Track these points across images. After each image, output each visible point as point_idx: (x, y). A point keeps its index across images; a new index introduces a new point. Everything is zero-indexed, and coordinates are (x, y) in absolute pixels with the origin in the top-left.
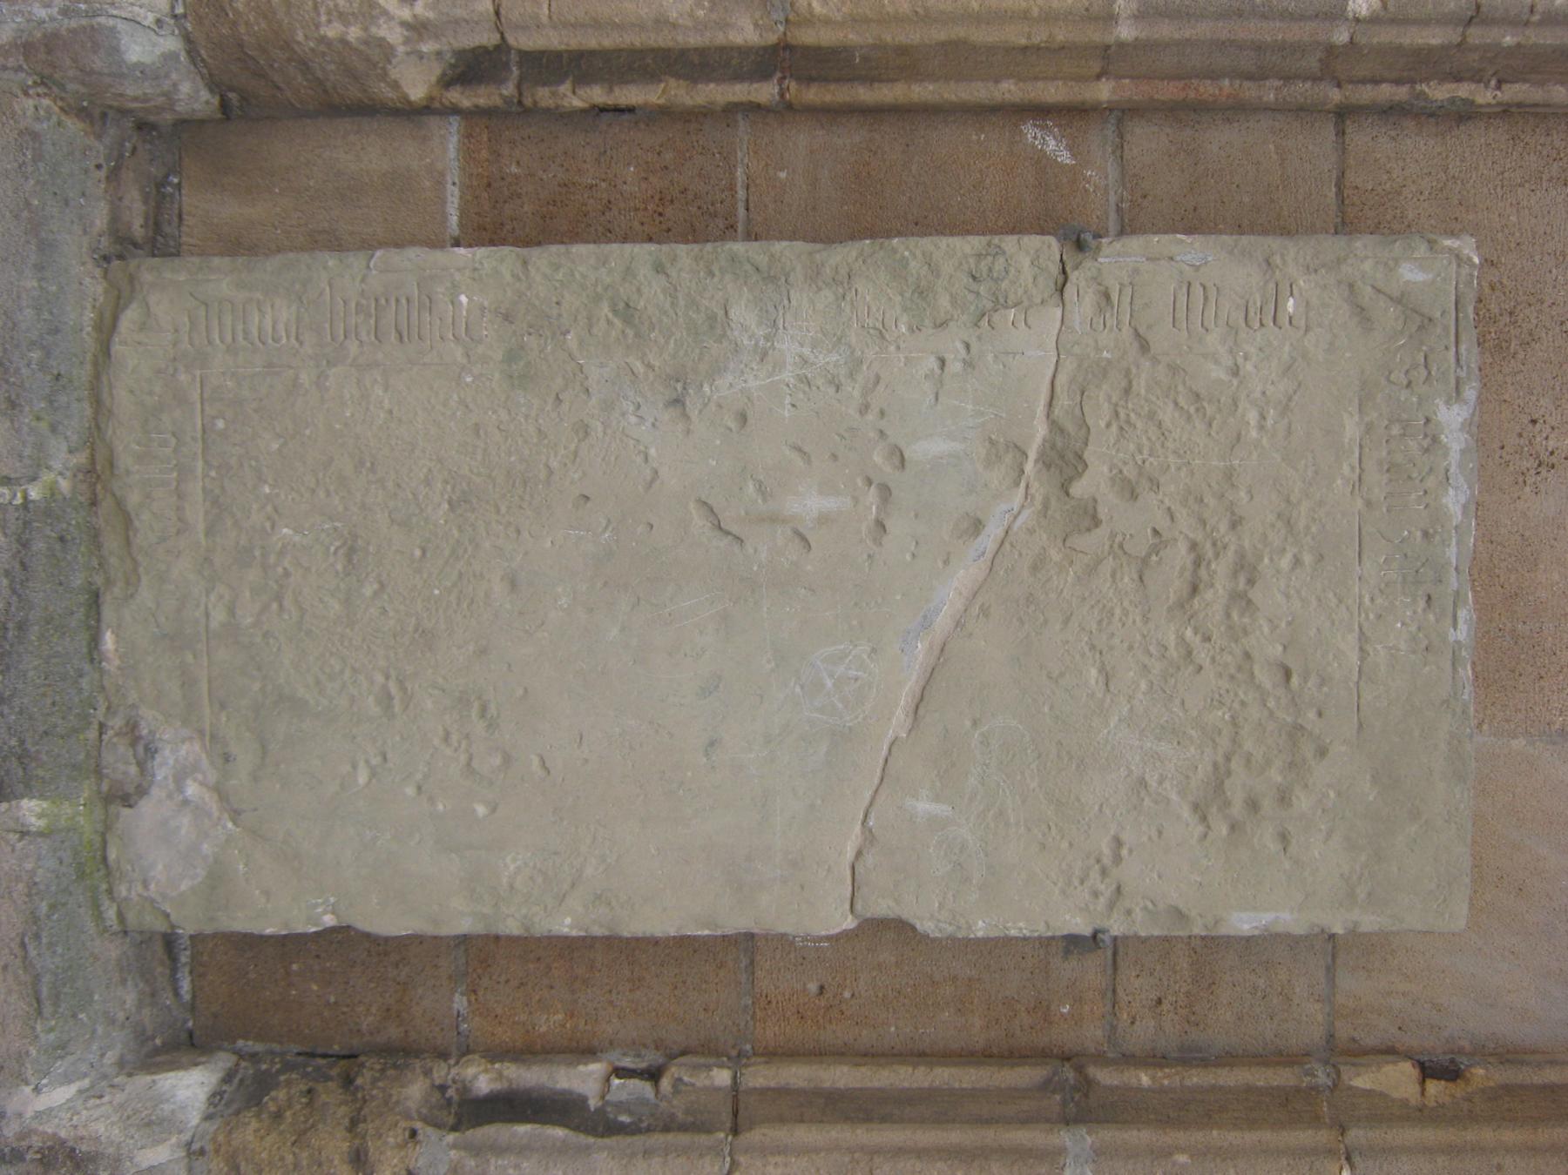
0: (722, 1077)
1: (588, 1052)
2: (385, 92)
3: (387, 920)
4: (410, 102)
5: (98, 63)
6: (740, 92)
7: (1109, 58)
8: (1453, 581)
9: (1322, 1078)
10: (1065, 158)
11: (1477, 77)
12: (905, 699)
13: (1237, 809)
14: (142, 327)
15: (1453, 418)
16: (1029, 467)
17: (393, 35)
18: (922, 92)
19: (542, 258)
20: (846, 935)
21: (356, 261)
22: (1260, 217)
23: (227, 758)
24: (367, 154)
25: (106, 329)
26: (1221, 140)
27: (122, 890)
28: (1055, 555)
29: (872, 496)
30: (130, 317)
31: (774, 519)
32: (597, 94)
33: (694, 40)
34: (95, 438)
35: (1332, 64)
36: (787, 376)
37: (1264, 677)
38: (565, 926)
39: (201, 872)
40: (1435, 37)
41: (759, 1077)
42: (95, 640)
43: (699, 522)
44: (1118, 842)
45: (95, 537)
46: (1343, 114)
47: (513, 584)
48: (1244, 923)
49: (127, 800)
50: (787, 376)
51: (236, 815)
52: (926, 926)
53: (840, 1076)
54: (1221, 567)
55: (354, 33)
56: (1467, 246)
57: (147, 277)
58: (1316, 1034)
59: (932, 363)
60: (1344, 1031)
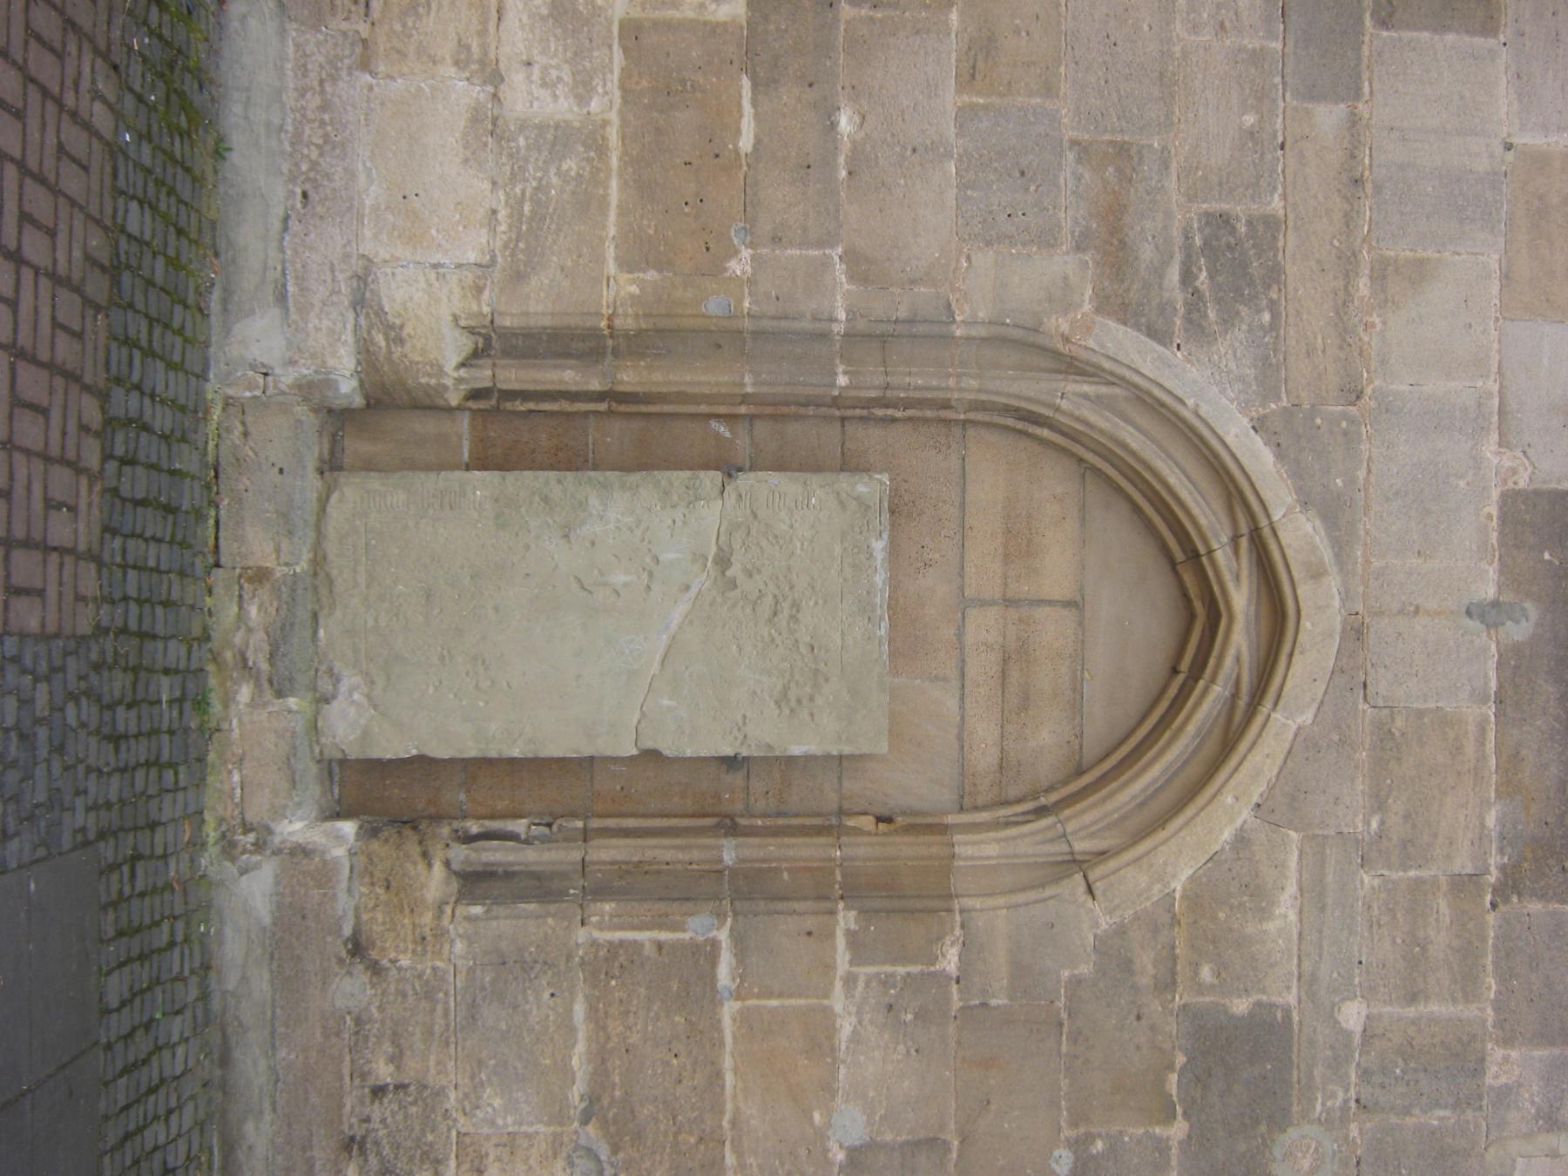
0: (580, 824)
1: (517, 816)
2: (441, 402)
3: (440, 751)
4: (1232, 1017)
5: (330, 394)
6: (591, 407)
7: (745, 399)
8: (879, 612)
9: (834, 821)
10: (728, 435)
11: (895, 407)
12: (658, 657)
13: (793, 703)
14: (341, 501)
15: (879, 546)
16: (709, 564)
17: (449, 382)
18: (667, 408)
19: (511, 476)
20: (632, 758)
21: (433, 475)
22: (810, 465)
23: (373, 683)
24: (427, 426)
25: (323, 502)
26: (792, 428)
27: (323, 740)
28: (719, 600)
29: (645, 576)
30: (335, 497)
31: (605, 584)
32: (531, 406)
33: (574, 388)
34: (318, 546)
35: (835, 402)
36: (611, 526)
37: (803, 650)
38: (516, 753)
39: (359, 732)
40: (873, 394)
41: (595, 823)
42: (315, 633)
43: (575, 586)
44: (745, 717)
45: (316, 588)
46: (843, 419)
47: (497, 609)
48: (796, 750)
49: (327, 701)
50: (611, 526)
51: (375, 707)
52: (667, 752)
53: (630, 823)
54: (786, 605)
55: (433, 381)
56: (885, 478)
57: (342, 480)
58: (835, 807)
59: (670, 522)
60: (846, 806)
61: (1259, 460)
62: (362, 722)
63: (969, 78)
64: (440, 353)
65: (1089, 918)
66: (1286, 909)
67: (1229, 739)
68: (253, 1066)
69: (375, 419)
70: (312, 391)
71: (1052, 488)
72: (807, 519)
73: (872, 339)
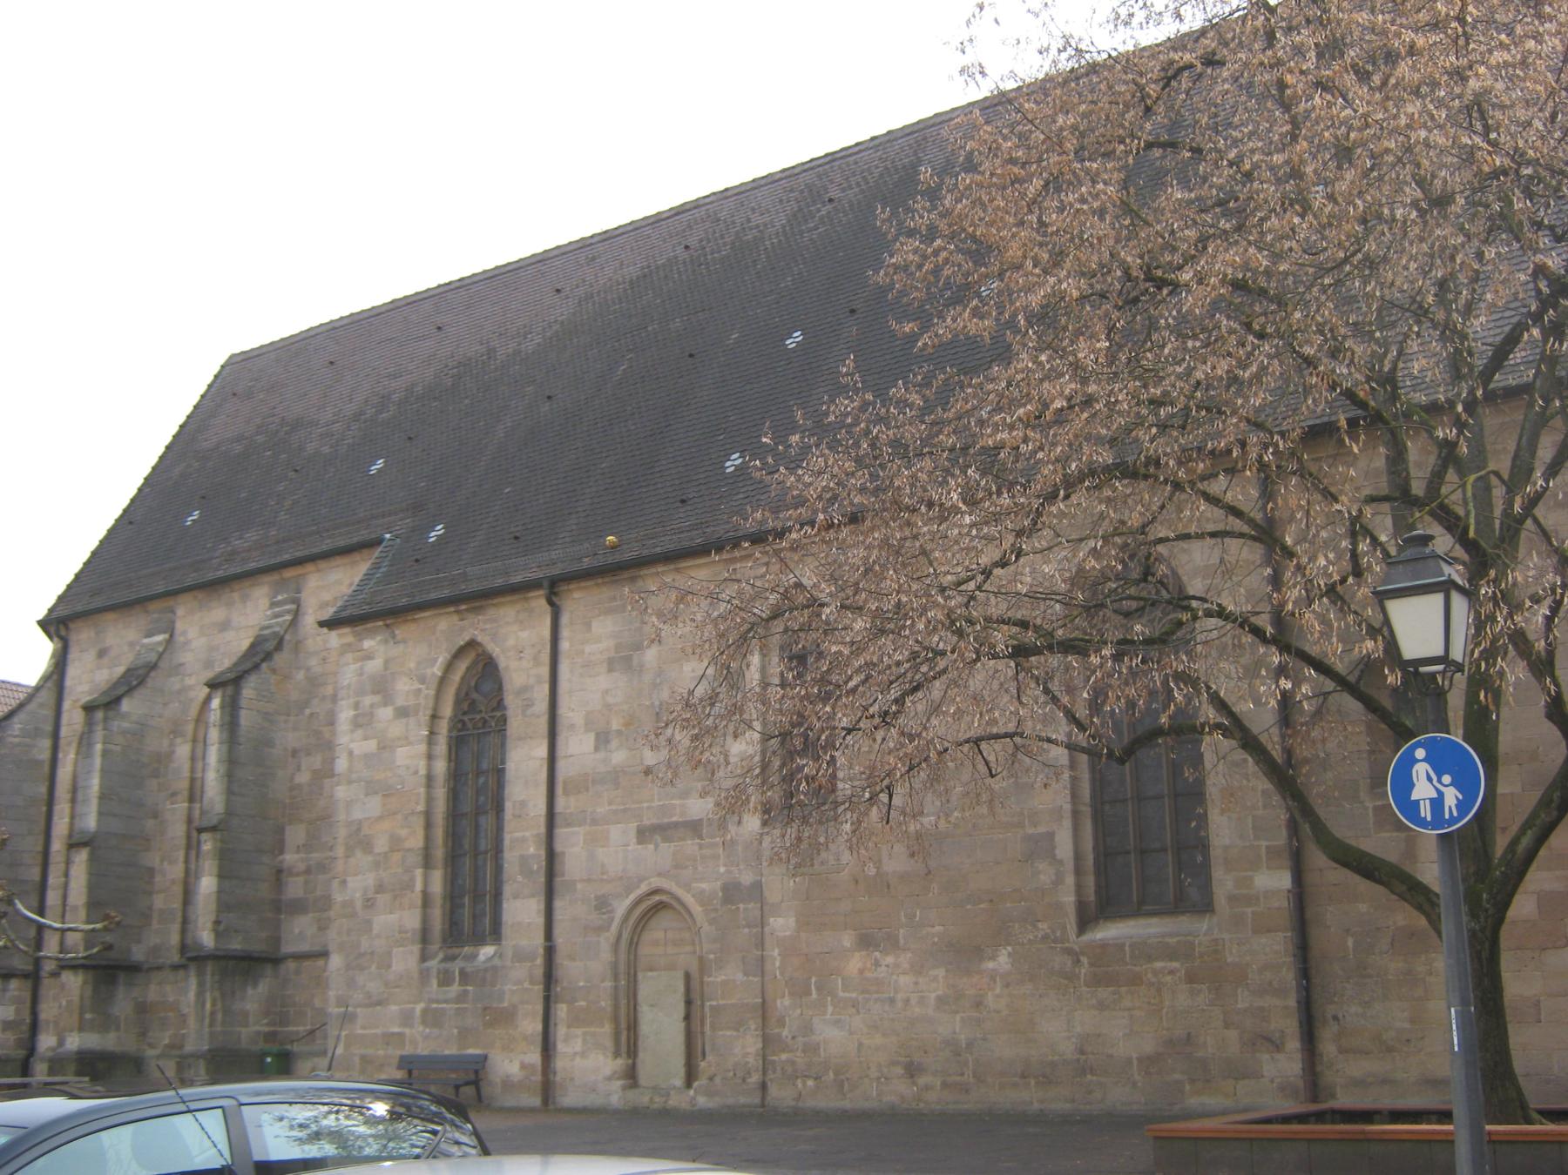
61: (632, 897)
62: (692, 1092)
63: (574, 960)
64: (620, 1063)
65: (706, 928)
66: (704, 886)
67: (678, 900)
68: (731, 1101)
69: (631, 1076)
70: (624, 1088)
71: (647, 936)
72: (645, 989)
73: (616, 977)
